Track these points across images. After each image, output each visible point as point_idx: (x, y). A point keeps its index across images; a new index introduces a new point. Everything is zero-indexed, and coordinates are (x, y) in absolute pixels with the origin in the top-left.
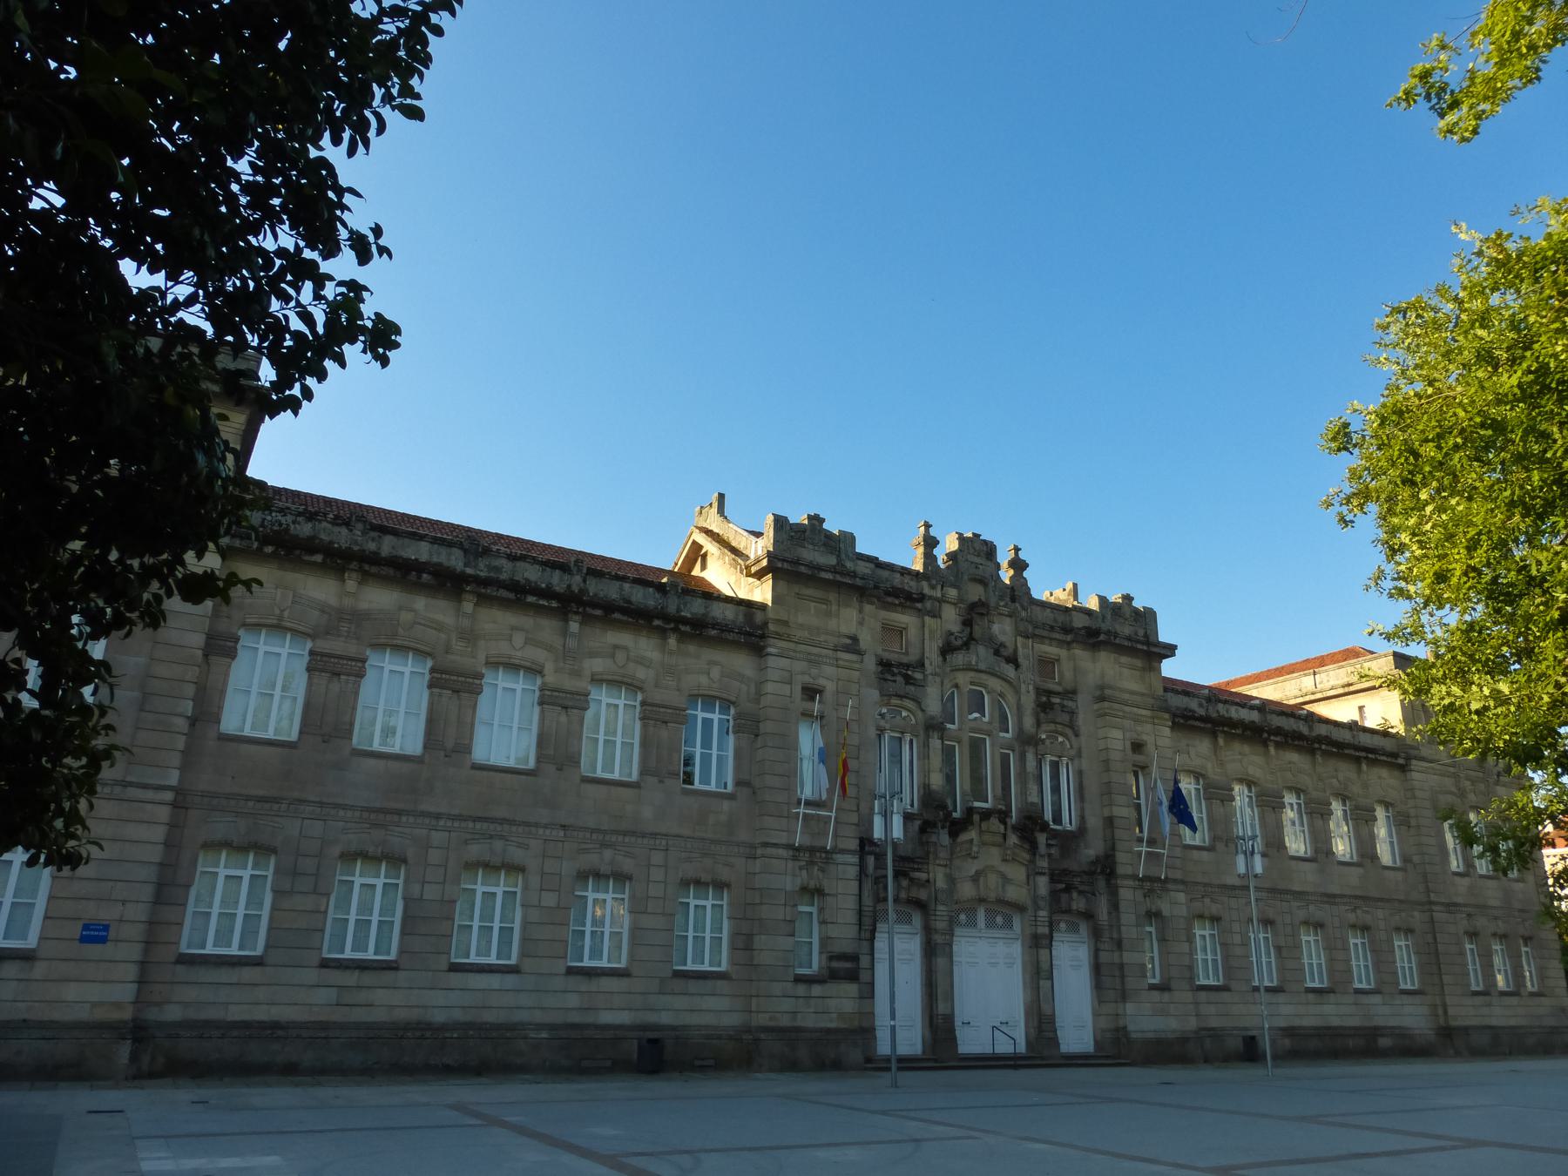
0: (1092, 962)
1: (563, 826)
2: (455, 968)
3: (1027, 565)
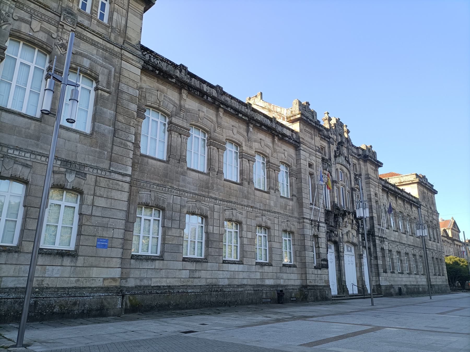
1: (252, 207)
2: (224, 262)
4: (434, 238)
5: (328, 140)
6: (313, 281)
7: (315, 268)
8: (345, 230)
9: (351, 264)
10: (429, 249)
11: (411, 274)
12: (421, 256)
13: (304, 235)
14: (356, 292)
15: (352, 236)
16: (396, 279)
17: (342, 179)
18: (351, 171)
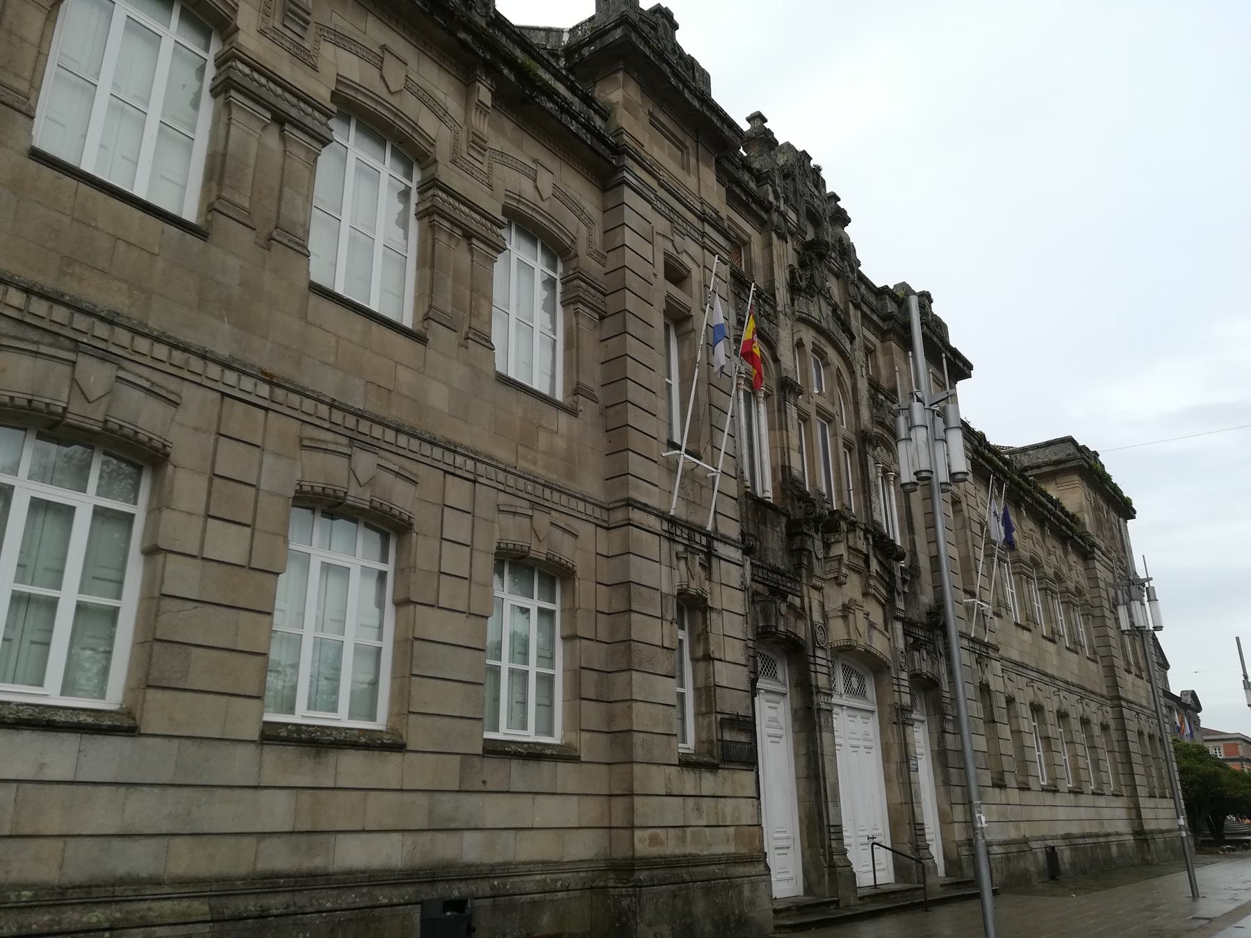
0: (826, 736)
1: (269, 379)
3: (849, 221)
4: (1137, 664)
5: (765, 217)
6: (672, 832)
7: (686, 763)
8: (836, 598)
9: (862, 750)
10: (1128, 701)
11: (1082, 793)
12: (1105, 727)
13: (627, 584)
14: (886, 876)
15: (866, 622)
16: (1037, 813)
17: (820, 388)
18: (858, 367)
